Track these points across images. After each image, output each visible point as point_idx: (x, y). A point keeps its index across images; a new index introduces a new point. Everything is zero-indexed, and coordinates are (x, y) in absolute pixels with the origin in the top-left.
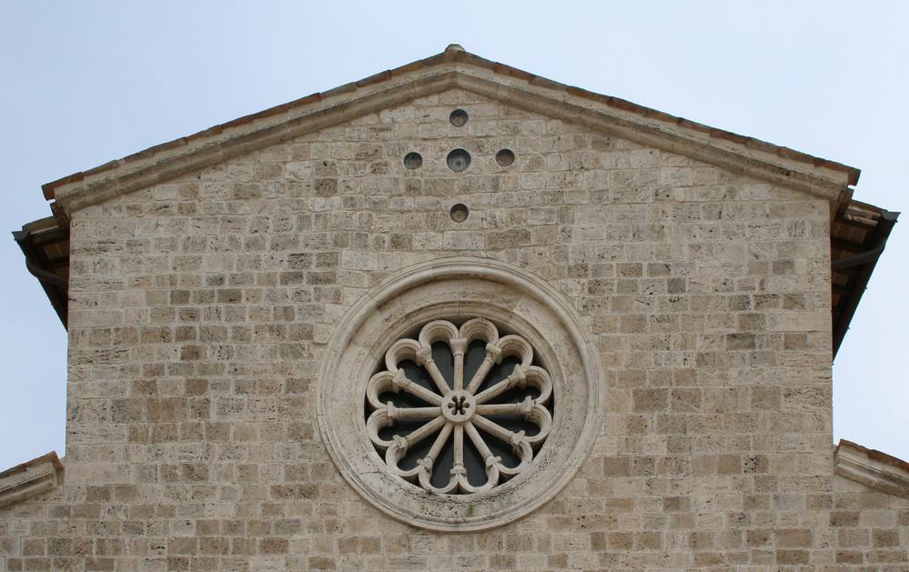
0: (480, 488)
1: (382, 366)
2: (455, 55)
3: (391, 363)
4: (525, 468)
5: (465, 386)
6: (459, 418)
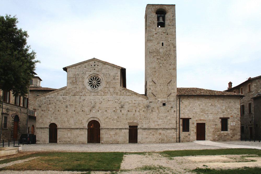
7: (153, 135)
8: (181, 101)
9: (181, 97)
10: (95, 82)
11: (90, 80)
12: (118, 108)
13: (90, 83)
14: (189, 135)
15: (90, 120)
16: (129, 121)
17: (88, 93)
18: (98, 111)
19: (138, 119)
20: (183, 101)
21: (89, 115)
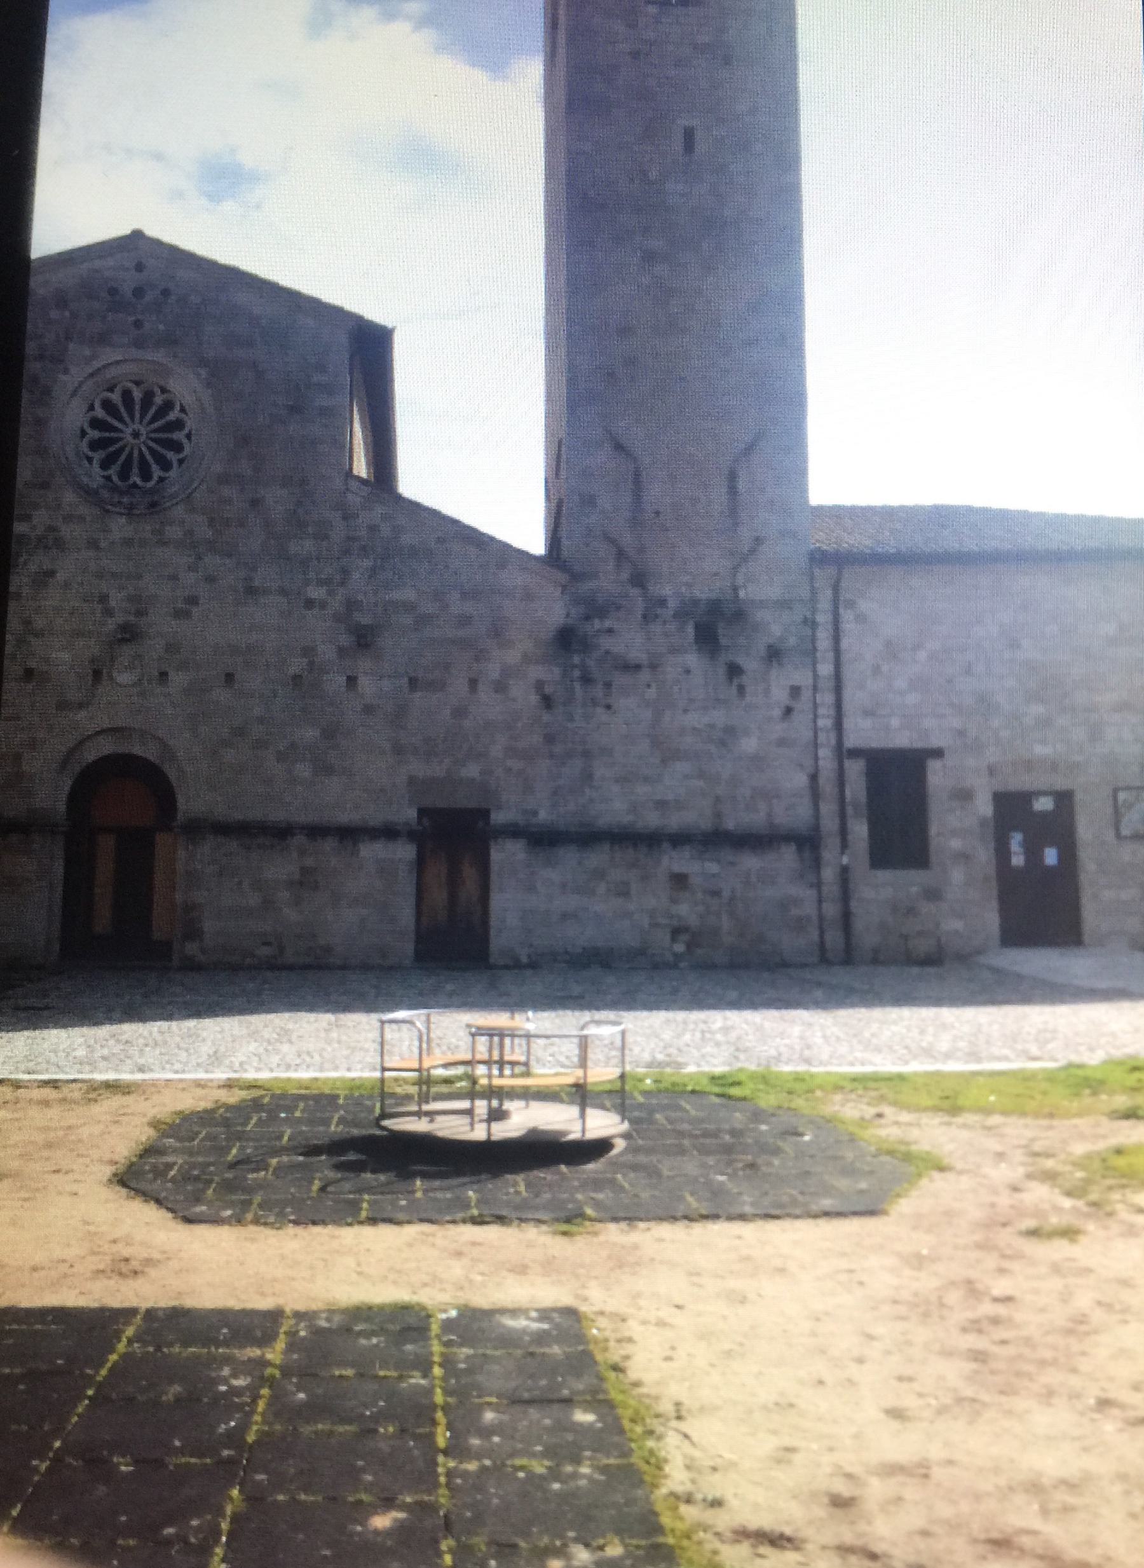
0: (148, 483)
1: (91, 408)
2: (137, 235)
3: (97, 405)
4: (173, 473)
5: (141, 422)
6: (136, 441)
7: (623, 892)
8: (851, 604)
9: (847, 573)
10: (136, 435)
11: (100, 413)
12: (326, 652)
13: (171, 455)
14: (933, 894)
15: (90, 755)
16: (418, 768)
17: (81, 519)
18: (163, 675)
19: (496, 751)
20: (864, 605)
21: (81, 706)
